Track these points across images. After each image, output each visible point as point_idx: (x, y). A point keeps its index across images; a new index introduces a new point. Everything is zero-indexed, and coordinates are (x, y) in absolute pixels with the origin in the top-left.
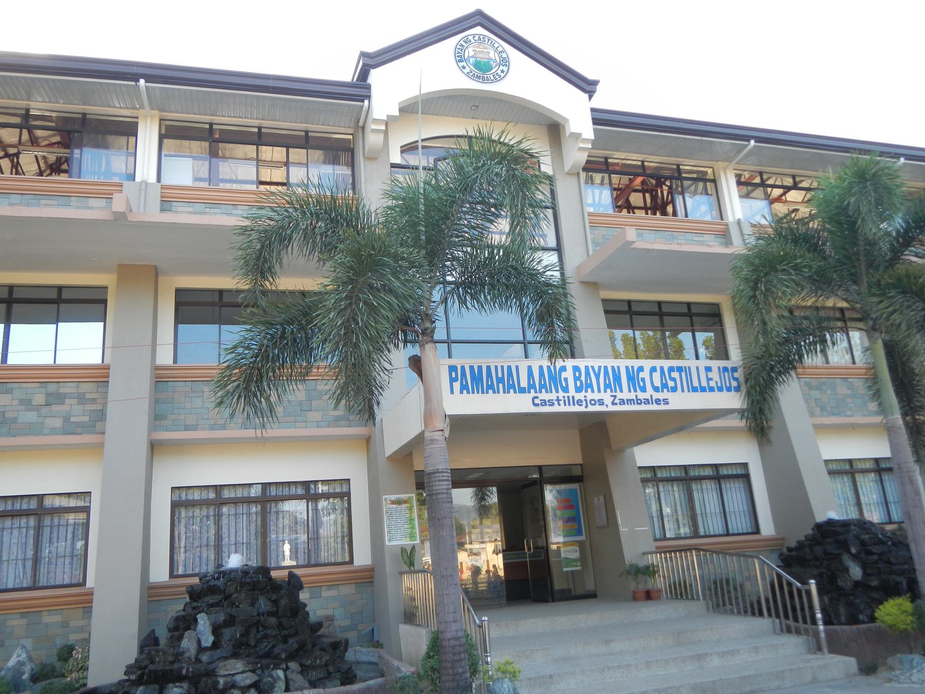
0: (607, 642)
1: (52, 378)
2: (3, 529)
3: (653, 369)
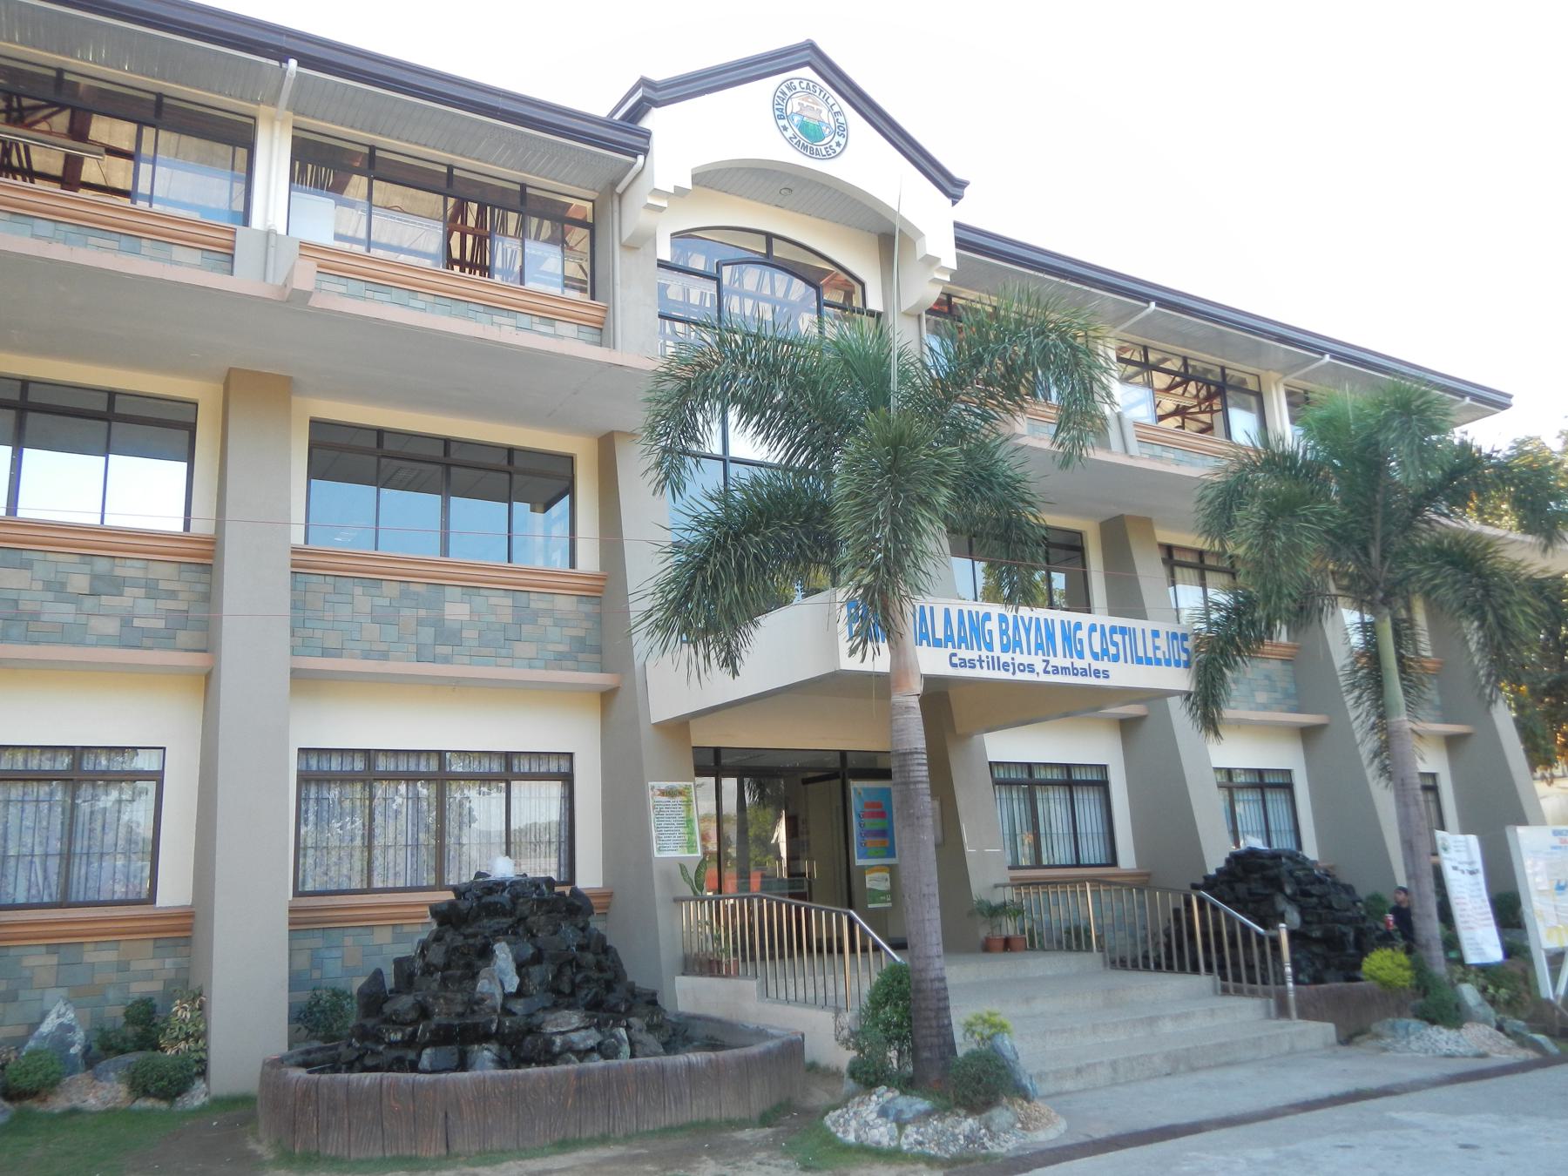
0: (1028, 1000)
1: (99, 546)
2: (7, 802)
3: (1093, 628)
